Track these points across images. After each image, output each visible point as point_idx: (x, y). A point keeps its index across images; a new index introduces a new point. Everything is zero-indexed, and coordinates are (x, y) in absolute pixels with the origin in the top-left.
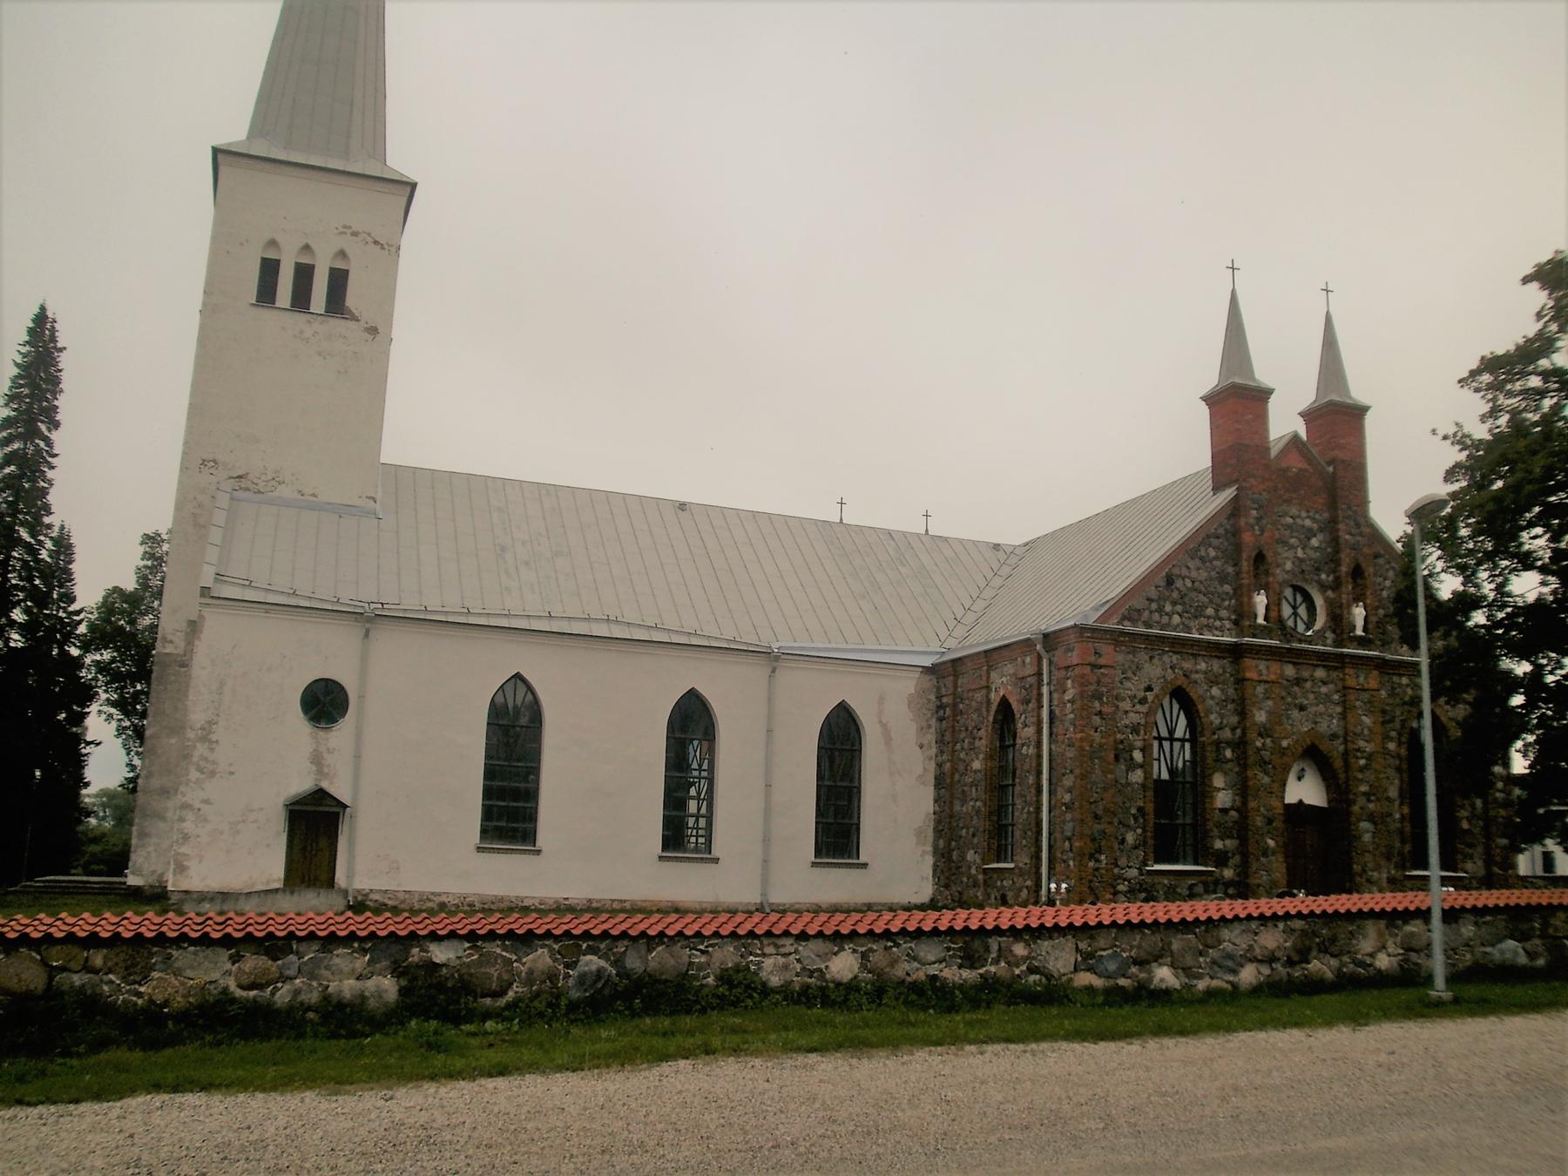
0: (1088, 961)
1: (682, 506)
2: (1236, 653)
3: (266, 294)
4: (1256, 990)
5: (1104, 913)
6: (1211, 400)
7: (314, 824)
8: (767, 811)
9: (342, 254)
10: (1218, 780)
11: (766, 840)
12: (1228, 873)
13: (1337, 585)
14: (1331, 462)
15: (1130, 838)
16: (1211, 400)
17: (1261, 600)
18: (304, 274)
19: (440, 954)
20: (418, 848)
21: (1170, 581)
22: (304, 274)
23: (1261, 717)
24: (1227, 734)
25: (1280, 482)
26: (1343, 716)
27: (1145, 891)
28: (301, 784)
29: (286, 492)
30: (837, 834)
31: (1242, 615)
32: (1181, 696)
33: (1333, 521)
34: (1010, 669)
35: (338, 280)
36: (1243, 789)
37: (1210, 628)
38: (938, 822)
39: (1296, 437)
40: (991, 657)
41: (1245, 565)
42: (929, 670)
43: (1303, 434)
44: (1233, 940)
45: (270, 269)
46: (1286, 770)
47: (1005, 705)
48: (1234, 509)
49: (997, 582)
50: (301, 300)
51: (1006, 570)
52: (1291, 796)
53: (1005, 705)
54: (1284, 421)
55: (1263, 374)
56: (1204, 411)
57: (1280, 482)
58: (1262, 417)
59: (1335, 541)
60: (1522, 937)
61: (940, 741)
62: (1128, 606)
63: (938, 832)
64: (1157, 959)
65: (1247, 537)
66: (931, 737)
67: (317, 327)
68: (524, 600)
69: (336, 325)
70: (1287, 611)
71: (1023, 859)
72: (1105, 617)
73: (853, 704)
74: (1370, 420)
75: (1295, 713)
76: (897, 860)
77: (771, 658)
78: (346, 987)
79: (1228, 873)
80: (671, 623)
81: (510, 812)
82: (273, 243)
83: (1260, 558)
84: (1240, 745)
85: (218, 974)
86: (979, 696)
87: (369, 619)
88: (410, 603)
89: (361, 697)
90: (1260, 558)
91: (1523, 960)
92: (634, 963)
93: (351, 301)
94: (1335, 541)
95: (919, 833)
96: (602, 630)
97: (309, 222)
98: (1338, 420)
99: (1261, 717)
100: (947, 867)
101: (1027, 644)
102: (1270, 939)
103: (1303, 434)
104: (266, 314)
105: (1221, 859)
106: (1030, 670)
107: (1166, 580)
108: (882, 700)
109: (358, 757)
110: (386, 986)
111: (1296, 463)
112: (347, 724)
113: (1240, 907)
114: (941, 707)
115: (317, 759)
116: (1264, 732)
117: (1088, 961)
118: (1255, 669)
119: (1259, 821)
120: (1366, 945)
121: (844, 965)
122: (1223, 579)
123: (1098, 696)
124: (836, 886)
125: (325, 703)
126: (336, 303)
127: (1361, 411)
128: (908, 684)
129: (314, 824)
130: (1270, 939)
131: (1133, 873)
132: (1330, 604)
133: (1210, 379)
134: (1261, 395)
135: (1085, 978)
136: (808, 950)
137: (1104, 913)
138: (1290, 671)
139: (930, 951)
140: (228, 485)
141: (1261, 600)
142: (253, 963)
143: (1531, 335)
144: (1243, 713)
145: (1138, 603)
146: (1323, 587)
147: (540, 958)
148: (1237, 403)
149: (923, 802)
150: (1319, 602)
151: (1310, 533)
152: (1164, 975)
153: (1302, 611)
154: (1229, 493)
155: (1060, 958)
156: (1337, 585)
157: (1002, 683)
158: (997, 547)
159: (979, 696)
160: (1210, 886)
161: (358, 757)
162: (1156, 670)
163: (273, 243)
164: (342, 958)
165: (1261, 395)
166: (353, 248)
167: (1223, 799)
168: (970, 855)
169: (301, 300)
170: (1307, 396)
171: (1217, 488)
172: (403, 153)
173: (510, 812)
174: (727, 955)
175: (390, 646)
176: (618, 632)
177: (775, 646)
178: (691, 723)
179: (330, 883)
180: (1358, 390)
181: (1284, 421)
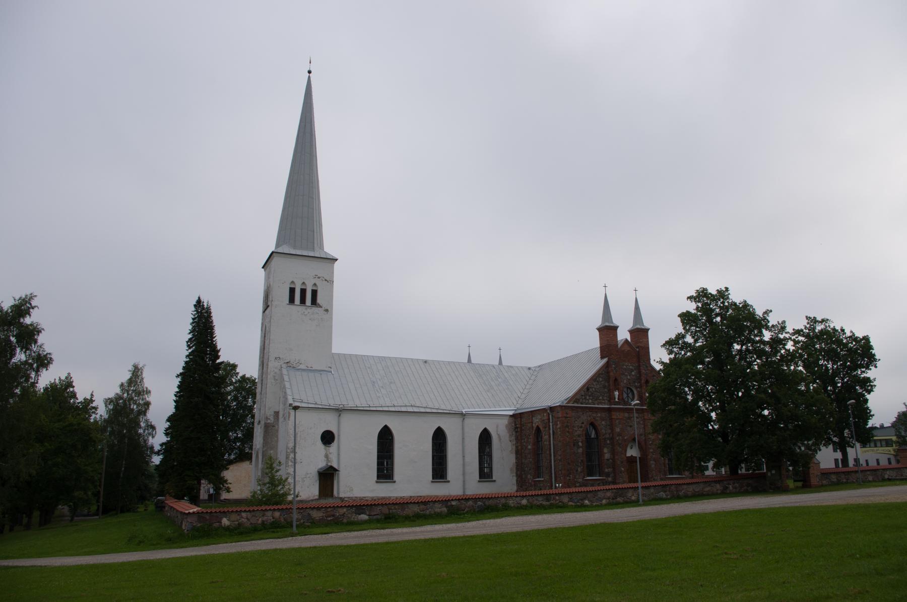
0: (571, 500)
1: (426, 362)
2: (609, 410)
3: (292, 300)
4: (606, 505)
5: (574, 490)
6: (600, 330)
7: (327, 476)
8: (464, 465)
9: (315, 285)
10: (605, 450)
11: (464, 474)
12: (610, 479)
13: (641, 387)
14: (638, 347)
15: (579, 469)
16: (600, 330)
17: (617, 393)
18: (303, 292)
19: (454, 503)
20: (358, 482)
21: (588, 389)
22: (303, 292)
23: (618, 430)
24: (607, 436)
25: (621, 353)
26: (644, 428)
27: (585, 484)
28: (322, 464)
29: (302, 367)
30: (485, 474)
31: (611, 399)
32: (592, 424)
33: (639, 366)
34: (539, 417)
35: (314, 293)
36: (613, 452)
37: (601, 403)
38: (517, 466)
39: (627, 340)
40: (533, 413)
41: (611, 383)
42: (513, 416)
43: (629, 339)
44: (600, 494)
45: (292, 291)
46: (626, 446)
47: (538, 428)
48: (607, 365)
49: (531, 382)
50: (303, 301)
51: (533, 377)
52: (629, 454)
53: (538, 428)
54: (623, 335)
55: (616, 321)
56: (597, 333)
57: (621, 353)
58: (616, 335)
59: (640, 372)
60: (665, 492)
61: (517, 439)
62: (576, 398)
63: (517, 469)
64: (585, 499)
65: (611, 374)
66: (513, 438)
67: (309, 311)
68: (385, 401)
69: (315, 309)
70: (625, 395)
71: (547, 477)
72: (568, 402)
73: (489, 428)
74: (650, 333)
75: (629, 428)
76: (504, 480)
77: (463, 415)
78: (438, 510)
79: (610, 479)
80: (431, 405)
81: (385, 472)
82: (293, 282)
83: (616, 380)
84: (612, 439)
85: (416, 509)
86: (529, 425)
87: (339, 411)
88: (351, 405)
89: (339, 436)
90: (616, 380)
91: (664, 496)
92: (487, 503)
93: (319, 301)
94: (640, 372)
95: (511, 470)
96: (410, 409)
97: (302, 274)
98: (640, 333)
99: (618, 430)
100: (522, 482)
101: (544, 410)
102: (609, 494)
103: (629, 339)
104: (292, 307)
105: (608, 475)
106: (545, 418)
107: (586, 390)
108: (497, 427)
109: (339, 455)
110: (445, 509)
111: (627, 348)
112: (334, 445)
113: (602, 488)
114: (516, 428)
115: (327, 456)
116: (619, 434)
117: (571, 500)
118: (615, 415)
119: (619, 462)
120: (629, 494)
121: (524, 502)
122: (604, 387)
123: (567, 426)
124: (485, 489)
125: (328, 438)
126: (314, 301)
127: (648, 330)
128: (505, 421)
129: (327, 476)
130: (609, 494)
131: (581, 480)
132: (638, 392)
133: (599, 322)
134: (615, 328)
135: (571, 503)
136: (518, 499)
137: (574, 490)
138: (626, 415)
139: (540, 499)
140: (284, 366)
141: (617, 393)
142: (422, 507)
143: (709, 291)
144: (612, 429)
145: (578, 397)
146: (636, 388)
147: (470, 503)
148: (607, 331)
149: (512, 459)
150: (635, 392)
151: (632, 371)
152: (586, 502)
153: (630, 395)
154: (605, 360)
155: (565, 499)
156: (641, 387)
157: (537, 421)
158: (529, 369)
159: (529, 425)
160: (604, 483)
161: (339, 455)
162: (585, 418)
163: (293, 282)
164: (437, 505)
165: (615, 328)
166: (318, 282)
167: (607, 456)
168: (529, 476)
169: (303, 301)
170: (630, 325)
171: (602, 358)
172: (330, 247)
173: (385, 472)
174: (503, 501)
175: (345, 417)
176: (416, 410)
177: (464, 411)
178: (439, 438)
179: (332, 495)
180: (646, 324)
181: (623, 335)
